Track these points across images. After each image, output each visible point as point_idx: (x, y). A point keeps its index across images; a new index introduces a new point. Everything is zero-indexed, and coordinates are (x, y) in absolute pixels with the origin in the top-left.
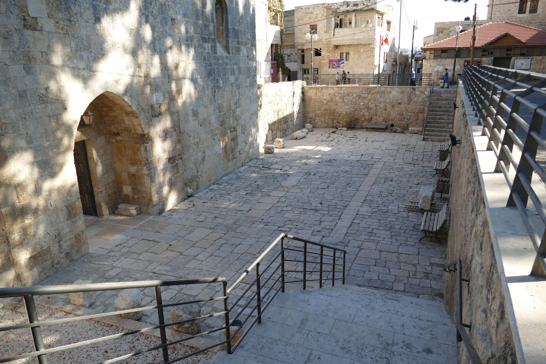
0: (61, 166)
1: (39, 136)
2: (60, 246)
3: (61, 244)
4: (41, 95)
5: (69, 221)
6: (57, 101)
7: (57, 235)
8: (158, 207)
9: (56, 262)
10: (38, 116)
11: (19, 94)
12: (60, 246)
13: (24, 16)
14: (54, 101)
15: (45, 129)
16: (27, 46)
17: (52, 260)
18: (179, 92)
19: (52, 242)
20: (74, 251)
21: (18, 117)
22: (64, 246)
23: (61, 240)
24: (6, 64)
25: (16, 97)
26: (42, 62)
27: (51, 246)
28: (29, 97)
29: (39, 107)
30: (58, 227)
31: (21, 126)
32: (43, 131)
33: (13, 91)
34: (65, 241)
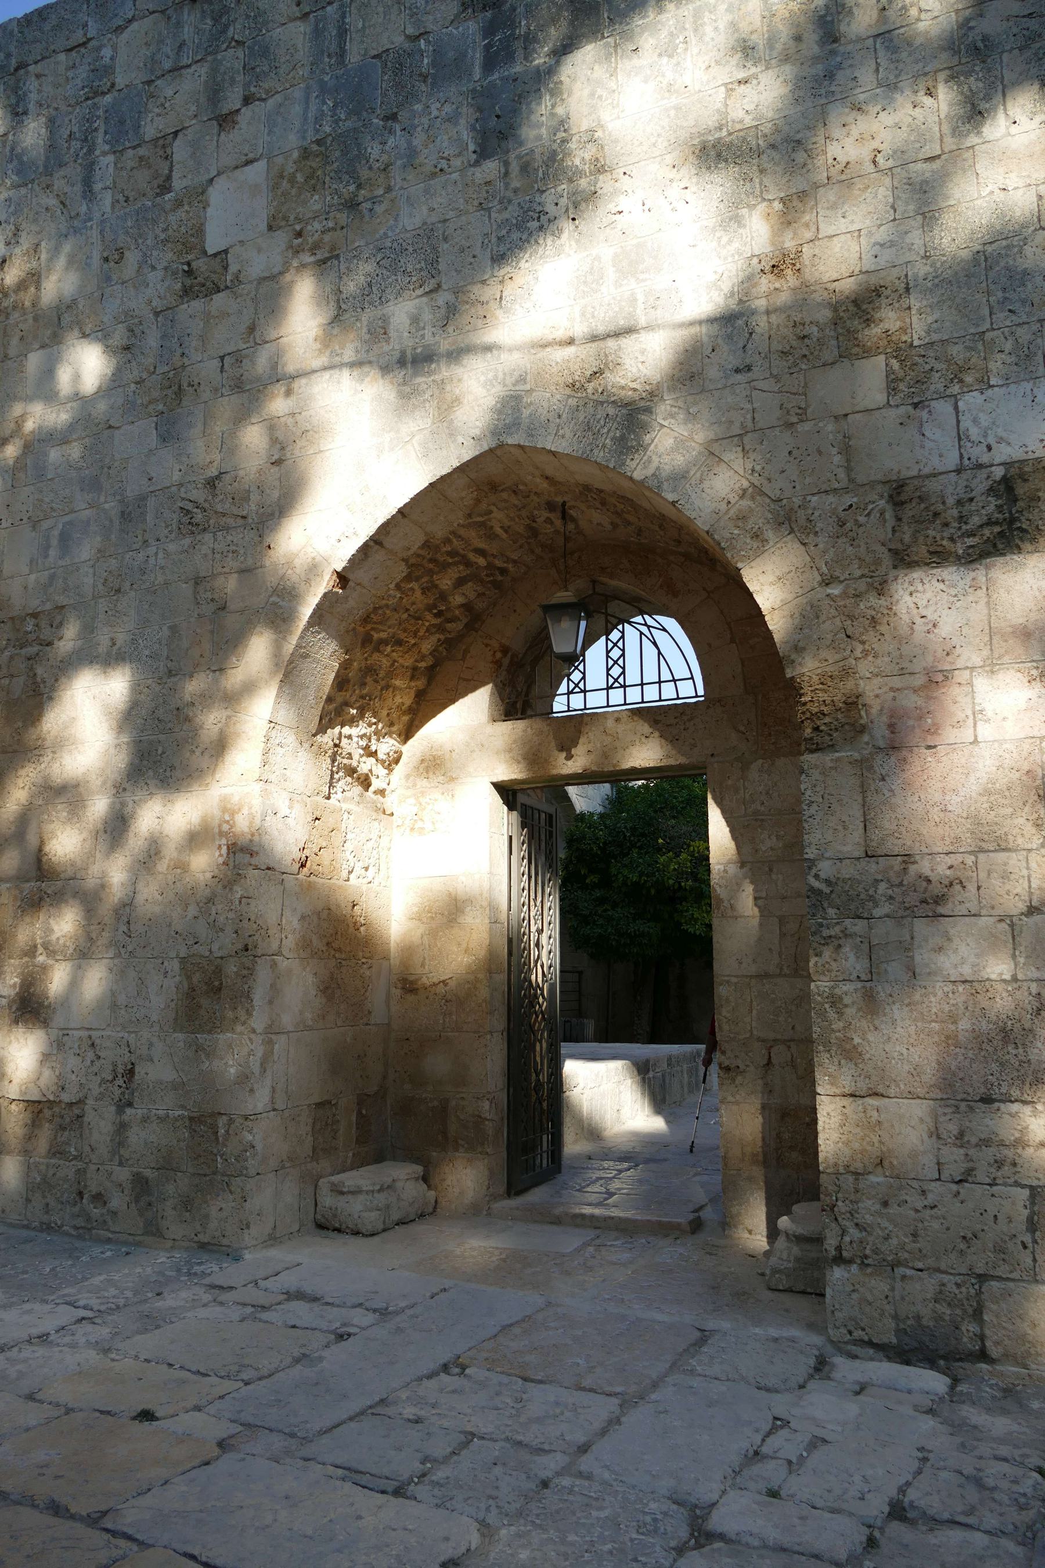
0: (220, 747)
1: (147, 652)
2: (122, 1127)
3: (125, 1118)
4: (189, 506)
5: (180, 1036)
6: (240, 522)
7: (120, 1069)
8: (879, 1285)
9: (93, 1188)
10: (160, 579)
11: (123, 513)
12: (122, 1127)
13: (189, 264)
14: (230, 521)
15: (174, 629)
16: (179, 351)
17: (80, 1165)
18: (156, 579)
19: (96, 1091)
20: (428, 332)
21: (101, 587)
22: (136, 1137)
23: (130, 1104)
24: (110, 427)
25: (111, 521)
26: (216, 390)
27: (90, 1102)
28: (149, 517)
29: (172, 547)
30: (132, 1038)
31: (102, 616)
32: (166, 632)
33: (107, 506)
34: (145, 1119)
